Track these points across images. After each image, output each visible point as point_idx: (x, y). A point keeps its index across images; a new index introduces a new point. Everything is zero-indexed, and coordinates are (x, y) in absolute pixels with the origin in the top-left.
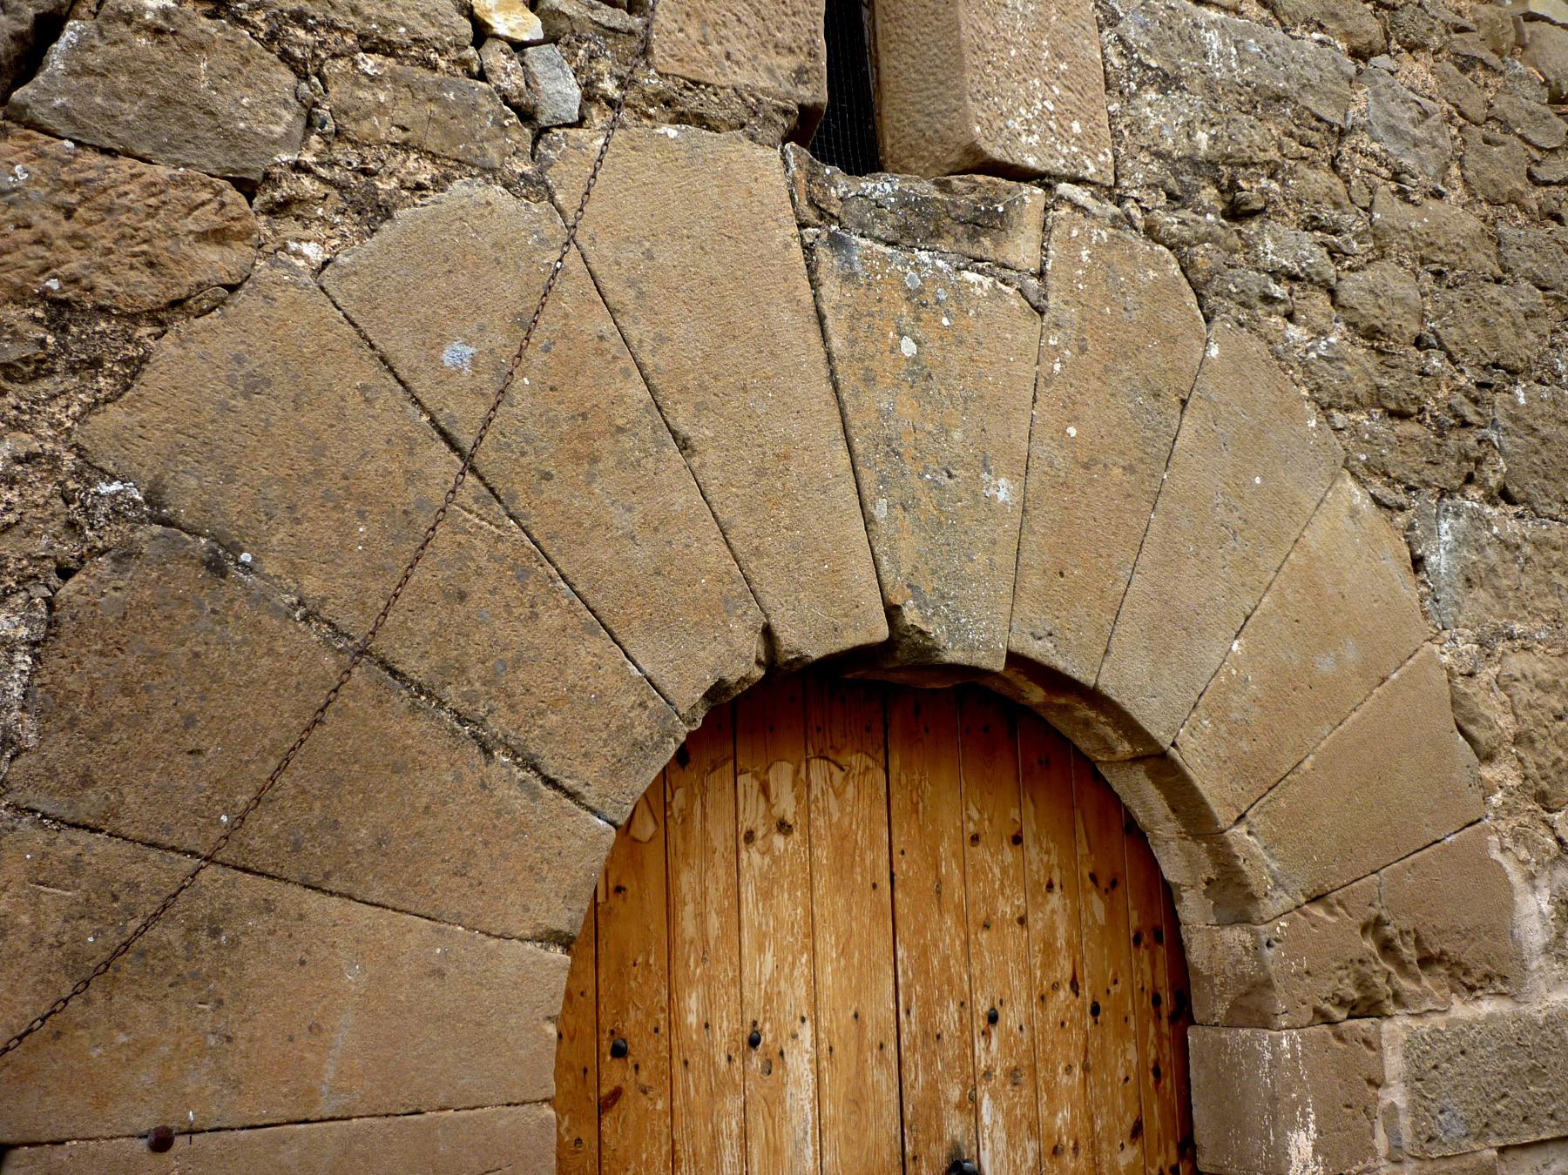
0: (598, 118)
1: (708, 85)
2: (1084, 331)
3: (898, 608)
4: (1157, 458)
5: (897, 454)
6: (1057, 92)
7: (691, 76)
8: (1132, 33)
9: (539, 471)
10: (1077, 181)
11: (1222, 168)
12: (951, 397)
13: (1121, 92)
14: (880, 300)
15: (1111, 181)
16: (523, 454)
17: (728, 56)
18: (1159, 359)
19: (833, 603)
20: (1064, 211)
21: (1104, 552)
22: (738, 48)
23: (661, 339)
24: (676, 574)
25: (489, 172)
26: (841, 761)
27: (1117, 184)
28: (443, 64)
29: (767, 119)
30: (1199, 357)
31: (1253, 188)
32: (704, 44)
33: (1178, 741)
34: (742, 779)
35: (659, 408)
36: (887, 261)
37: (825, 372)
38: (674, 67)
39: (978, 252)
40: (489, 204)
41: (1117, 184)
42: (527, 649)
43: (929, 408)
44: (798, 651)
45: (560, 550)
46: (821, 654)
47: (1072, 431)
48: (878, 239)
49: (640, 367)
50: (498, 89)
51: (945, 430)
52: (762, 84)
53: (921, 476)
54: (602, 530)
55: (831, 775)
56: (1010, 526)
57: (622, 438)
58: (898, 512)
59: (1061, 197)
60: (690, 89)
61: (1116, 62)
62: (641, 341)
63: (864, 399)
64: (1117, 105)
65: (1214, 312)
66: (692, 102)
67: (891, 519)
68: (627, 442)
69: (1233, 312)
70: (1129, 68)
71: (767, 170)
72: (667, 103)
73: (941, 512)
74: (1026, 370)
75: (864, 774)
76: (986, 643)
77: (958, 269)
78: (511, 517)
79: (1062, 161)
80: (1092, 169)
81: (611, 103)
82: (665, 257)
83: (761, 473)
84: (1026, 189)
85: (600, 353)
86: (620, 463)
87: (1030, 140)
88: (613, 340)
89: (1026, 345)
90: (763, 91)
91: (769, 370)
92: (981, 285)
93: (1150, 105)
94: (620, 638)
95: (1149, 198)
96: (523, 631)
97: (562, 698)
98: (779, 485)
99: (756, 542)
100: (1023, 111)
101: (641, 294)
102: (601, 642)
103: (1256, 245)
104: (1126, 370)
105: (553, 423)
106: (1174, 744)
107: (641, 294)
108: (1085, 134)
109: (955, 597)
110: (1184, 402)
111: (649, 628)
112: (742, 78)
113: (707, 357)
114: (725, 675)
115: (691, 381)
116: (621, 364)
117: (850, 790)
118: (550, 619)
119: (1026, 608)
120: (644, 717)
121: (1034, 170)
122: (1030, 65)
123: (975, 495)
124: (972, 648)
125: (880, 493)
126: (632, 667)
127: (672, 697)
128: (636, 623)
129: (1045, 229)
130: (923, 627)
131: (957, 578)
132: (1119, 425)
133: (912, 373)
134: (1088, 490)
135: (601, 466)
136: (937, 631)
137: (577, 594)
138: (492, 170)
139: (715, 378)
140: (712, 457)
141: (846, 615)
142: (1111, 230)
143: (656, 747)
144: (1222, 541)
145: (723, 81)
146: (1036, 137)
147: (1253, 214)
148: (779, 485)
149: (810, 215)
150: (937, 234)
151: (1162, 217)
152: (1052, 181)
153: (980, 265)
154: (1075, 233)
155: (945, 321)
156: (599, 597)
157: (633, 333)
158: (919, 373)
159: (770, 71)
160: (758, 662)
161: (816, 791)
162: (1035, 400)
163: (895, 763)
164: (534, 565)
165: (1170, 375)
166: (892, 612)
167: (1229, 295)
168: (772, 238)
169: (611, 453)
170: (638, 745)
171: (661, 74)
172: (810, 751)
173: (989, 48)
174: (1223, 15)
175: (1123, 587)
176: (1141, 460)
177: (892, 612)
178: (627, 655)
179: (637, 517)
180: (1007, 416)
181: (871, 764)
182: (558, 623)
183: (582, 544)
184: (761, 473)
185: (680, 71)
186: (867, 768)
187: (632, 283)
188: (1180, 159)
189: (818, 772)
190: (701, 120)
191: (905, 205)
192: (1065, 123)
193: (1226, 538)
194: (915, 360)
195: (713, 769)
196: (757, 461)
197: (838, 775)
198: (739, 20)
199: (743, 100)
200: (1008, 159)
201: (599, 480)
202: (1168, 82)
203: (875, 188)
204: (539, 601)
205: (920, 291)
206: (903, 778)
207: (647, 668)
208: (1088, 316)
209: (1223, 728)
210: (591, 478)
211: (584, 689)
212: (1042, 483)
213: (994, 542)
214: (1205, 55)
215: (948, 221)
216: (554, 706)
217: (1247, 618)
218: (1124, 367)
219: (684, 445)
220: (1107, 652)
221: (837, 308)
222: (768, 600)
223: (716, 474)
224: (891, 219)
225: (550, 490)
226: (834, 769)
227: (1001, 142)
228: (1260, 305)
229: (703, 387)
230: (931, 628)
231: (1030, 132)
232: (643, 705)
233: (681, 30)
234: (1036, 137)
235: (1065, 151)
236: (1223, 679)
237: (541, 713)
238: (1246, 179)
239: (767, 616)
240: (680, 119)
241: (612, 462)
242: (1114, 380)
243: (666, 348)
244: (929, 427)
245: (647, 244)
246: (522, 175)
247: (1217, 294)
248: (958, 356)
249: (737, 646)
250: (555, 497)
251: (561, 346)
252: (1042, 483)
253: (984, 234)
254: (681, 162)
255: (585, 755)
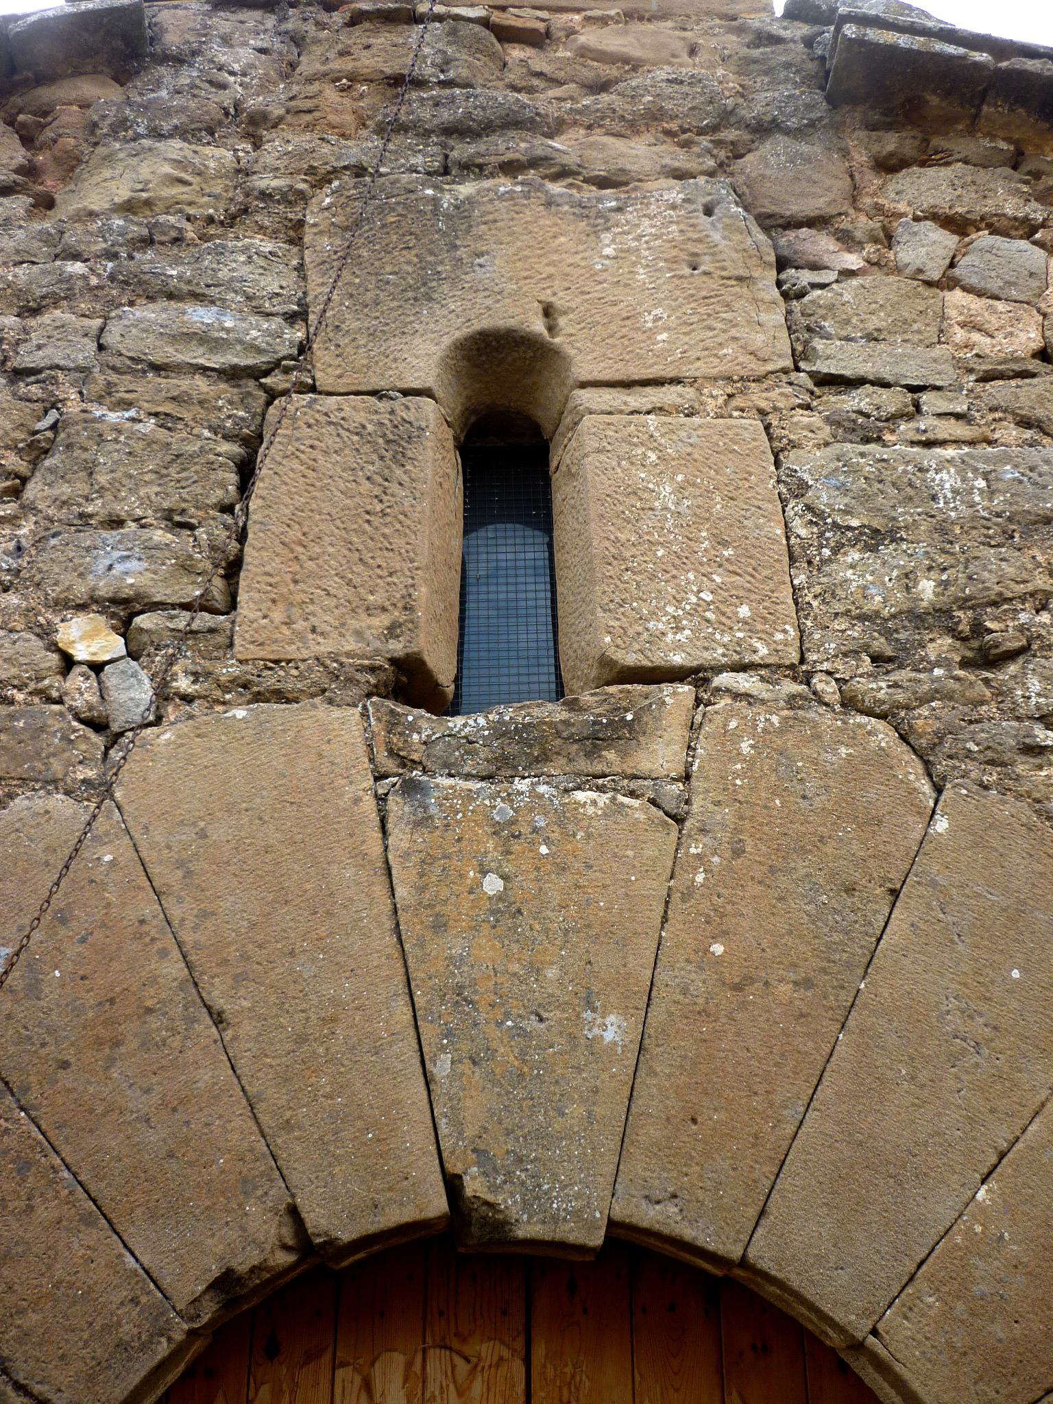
0: (171, 712)
1: (289, 662)
2: (741, 832)
3: (459, 1177)
4: (849, 965)
5: (471, 1002)
6: (718, 580)
7: (272, 657)
8: (825, 498)
9: (57, 1061)
10: (741, 668)
11: (960, 613)
12: (546, 931)
13: (810, 563)
14: (459, 840)
15: (794, 657)
16: (43, 1045)
17: (314, 630)
18: (855, 846)
19: (374, 1176)
20: (724, 702)
21: (760, 1089)
22: (324, 620)
23: (204, 915)
24: (191, 1156)
25: (52, 783)
26: (468, 1350)
27: (802, 661)
28: (20, 697)
29: (350, 680)
30: (917, 835)
31: (1003, 630)
32: (288, 623)
33: (881, 1327)
34: (340, 1373)
35: (196, 984)
36: (469, 796)
37: (389, 924)
38: (255, 652)
39: (599, 768)
40: (47, 812)
41: (802, 661)
42: (17, 1244)
43: (515, 948)
44: (326, 1234)
45: (66, 1138)
46: (354, 1236)
47: (718, 949)
48: (468, 777)
49: (180, 945)
50: (71, 709)
51: (536, 969)
52: (348, 648)
53: (500, 1024)
54: (115, 1115)
55: (453, 1367)
56: (621, 1070)
57: (149, 1018)
58: (466, 1067)
59: (718, 689)
60: (270, 669)
61: (803, 532)
62: (183, 920)
63: (432, 948)
64: (803, 577)
65: (944, 778)
66: (270, 680)
67: (454, 1076)
68: (154, 1022)
69: (973, 775)
70: (821, 535)
71: (342, 731)
72: (245, 687)
73: (524, 1062)
74: (656, 887)
75: (497, 1366)
76: (577, 1214)
77: (566, 791)
78: (22, 1109)
79: (720, 651)
80: (763, 651)
81: (188, 699)
82: (218, 833)
83: (301, 1039)
84: (667, 688)
85: (139, 936)
86: (143, 1044)
87: (678, 637)
88: (155, 922)
89: (655, 860)
90: (348, 655)
91: (323, 931)
92: (594, 803)
93: (852, 567)
94: (119, 1228)
95: (842, 668)
96: (15, 1225)
97: (48, 1295)
98: (321, 1050)
99: (288, 1114)
100: (670, 609)
101: (189, 874)
102: (98, 1234)
103: (1011, 690)
104: (802, 866)
105: (79, 1012)
106: (874, 1332)
107: (189, 874)
108: (756, 616)
109: (536, 1159)
110: (895, 893)
111: (152, 1216)
112: (325, 647)
113: (253, 925)
114: (234, 1264)
115: (233, 953)
116: (159, 945)
117: (478, 1387)
118: (45, 1212)
119: (636, 1166)
120: (134, 1314)
121: (681, 667)
122: (681, 561)
123: (572, 1037)
124: (555, 1219)
125: (443, 1049)
126: (129, 1259)
127: (169, 1292)
128: (139, 1211)
129: (693, 727)
130: (490, 1198)
131: (541, 1136)
132: (790, 933)
133: (493, 912)
134: (739, 1016)
135: (123, 1050)
136: (509, 1202)
137: (80, 1183)
138: (54, 781)
139: (260, 946)
140: (247, 1028)
141: (390, 1189)
142: (785, 713)
143: (143, 1348)
144: (954, 1059)
145: (305, 654)
146: (687, 632)
147: (1012, 655)
148: (321, 1050)
149: (390, 765)
150: (544, 758)
151: (862, 685)
152: (709, 675)
153: (600, 781)
154: (733, 724)
155: (544, 850)
156: (103, 1185)
157: (175, 912)
158: (505, 910)
159: (359, 634)
160: (285, 1247)
161: (433, 1388)
162: (665, 919)
163: (539, 1352)
164: (38, 1156)
165: (872, 863)
166: (453, 1184)
167: (969, 754)
168: (341, 796)
169: (135, 1035)
170: (122, 1346)
171: (241, 662)
172: (429, 1340)
173: (628, 554)
174: (966, 449)
175: (790, 1129)
176: (824, 971)
177: (453, 1184)
178: (125, 1246)
179: (155, 1098)
180: (624, 943)
181: (506, 1353)
182: (55, 1214)
183: (91, 1131)
184: (301, 1039)
185: (261, 654)
186: (501, 1359)
187: (180, 864)
188: (893, 616)
189: (437, 1364)
190: (280, 696)
191: (503, 735)
192: (728, 610)
193: (963, 1052)
194: (500, 898)
195: (306, 1363)
196: (299, 1027)
197: (462, 1367)
198: (328, 594)
199: (326, 667)
200: (646, 663)
201: (119, 1063)
202: (874, 539)
203: (465, 725)
204: (37, 1194)
205: (513, 822)
206: (550, 1372)
207: (145, 1260)
208: (748, 814)
209: (960, 1306)
210: (111, 1061)
211: (71, 1285)
212: (670, 1014)
213: (596, 1091)
214: (934, 498)
215: (558, 742)
216: (35, 1305)
217: (1002, 1155)
218: (801, 864)
219: (219, 1019)
220: (762, 1213)
221: (406, 855)
222: (294, 1178)
223: (248, 1045)
224: (484, 753)
225: (65, 1079)
226: (458, 1360)
227: (637, 647)
228: (1020, 758)
229: (245, 957)
230: (500, 1199)
231: (678, 629)
232: (135, 1301)
233: (265, 617)
234: (687, 632)
235: (726, 639)
236: (959, 1239)
237: (21, 1312)
238: (996, 619)
239: (293, 1196)
240: (258, 698)
241: (134, 1044)
242: (783, 881)
243: (209, 924)
244: (515, 967)
245: (202, 824)
246: (84, 781)
247: (950, 757)
248: (555, 888)
249: (250, 1231)
250: (70, 1086)
251: (98, 935)
252: (670, 1014)
253: (607, 748)
254: (248, 740)
255: (62, 1357)
